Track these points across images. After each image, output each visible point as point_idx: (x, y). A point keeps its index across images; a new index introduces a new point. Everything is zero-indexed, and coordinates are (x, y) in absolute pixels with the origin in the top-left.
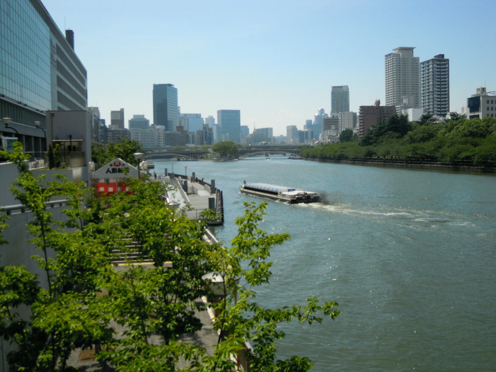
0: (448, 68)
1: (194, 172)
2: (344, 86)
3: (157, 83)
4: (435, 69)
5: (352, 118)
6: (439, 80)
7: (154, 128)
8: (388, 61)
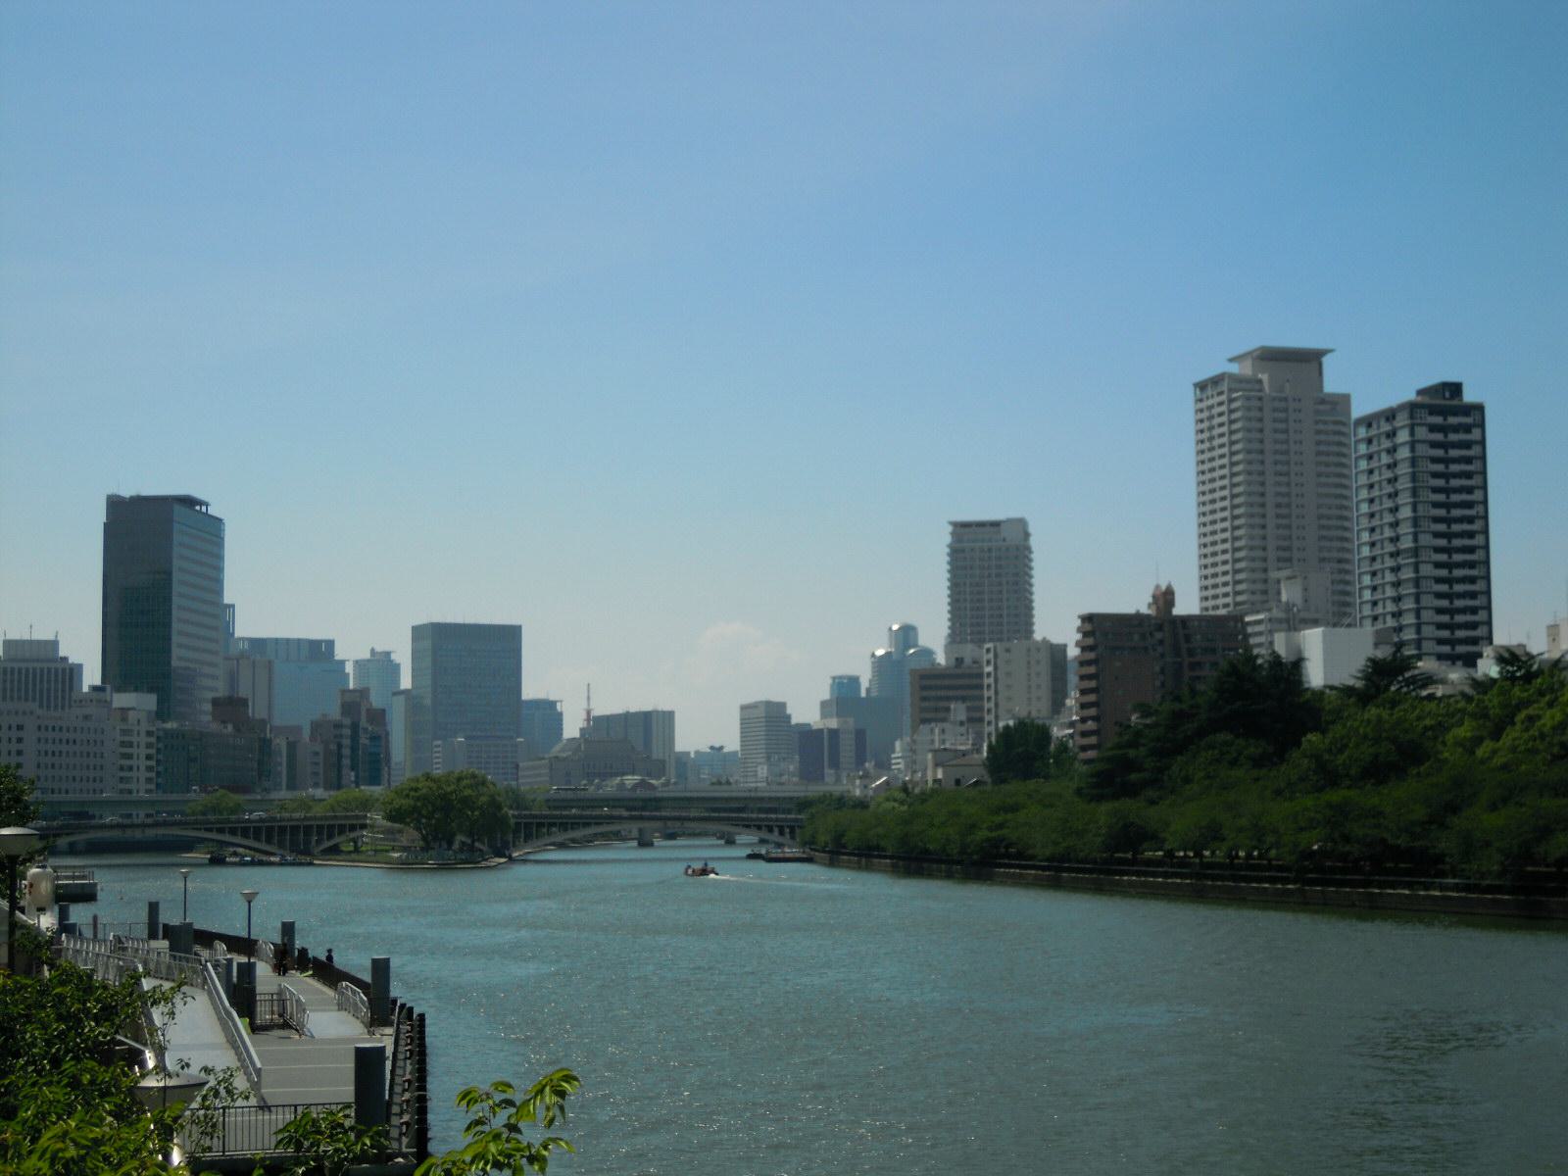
2: (1010, 521)
3: (127, 492)
4: (1423, 450)
6: (1441, 497)
8: (1210, 408)
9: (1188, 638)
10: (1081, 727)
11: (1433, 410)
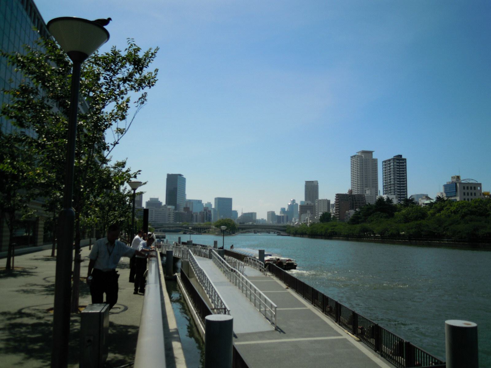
0: (406, 165)
1: (216, 240)
2: (315, 181)
3: (170, 173)
4: (396, 166)
5: (326, 204)
6: (399, 175)
7: (166, 207)
8: (353, 161)
9: (355, 198)
10: (336, 214)
11: (397, 160)
